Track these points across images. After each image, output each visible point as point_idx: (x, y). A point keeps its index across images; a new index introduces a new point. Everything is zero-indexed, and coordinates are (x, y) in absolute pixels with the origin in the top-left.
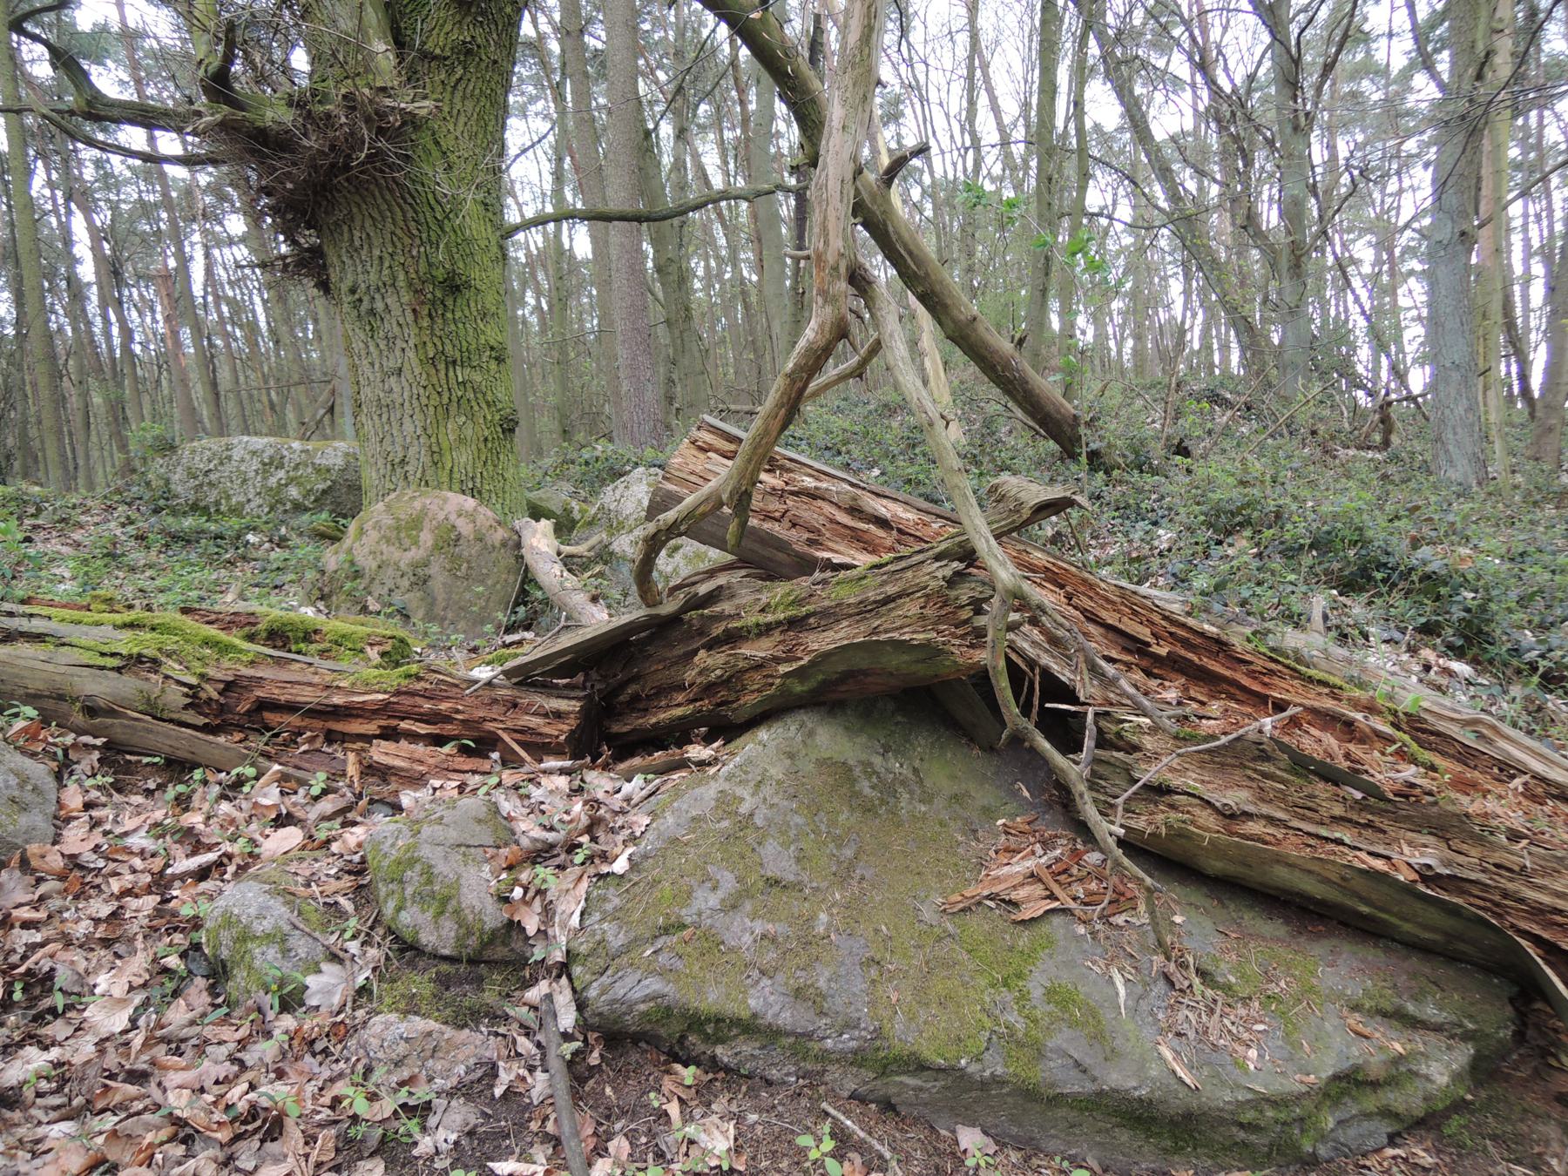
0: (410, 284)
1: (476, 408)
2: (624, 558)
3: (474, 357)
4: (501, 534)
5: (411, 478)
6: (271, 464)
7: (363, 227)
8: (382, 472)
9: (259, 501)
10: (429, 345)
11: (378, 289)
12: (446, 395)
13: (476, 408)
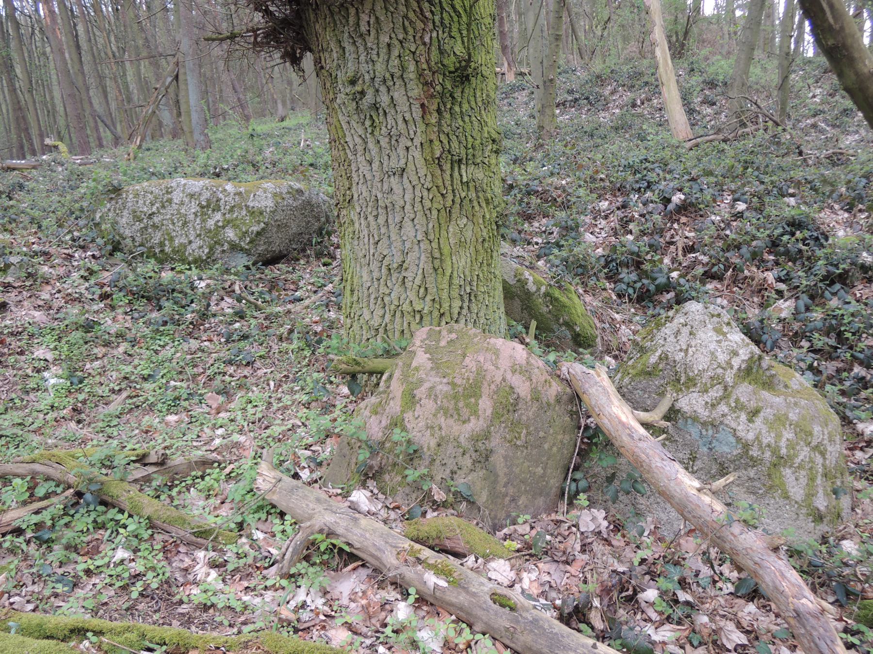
0: (420, 75)
1: (477, 208)
2: (695, 419)
3: (478, 153)
4: (555, 388)
5: (409, 284)
6: (208, 206)
7: (373, 10)
8: (376, 275)
9: (199, 242)
10: (437, 143)
11: (384, 81)
12: (450, 197)
13: (477, 208)
